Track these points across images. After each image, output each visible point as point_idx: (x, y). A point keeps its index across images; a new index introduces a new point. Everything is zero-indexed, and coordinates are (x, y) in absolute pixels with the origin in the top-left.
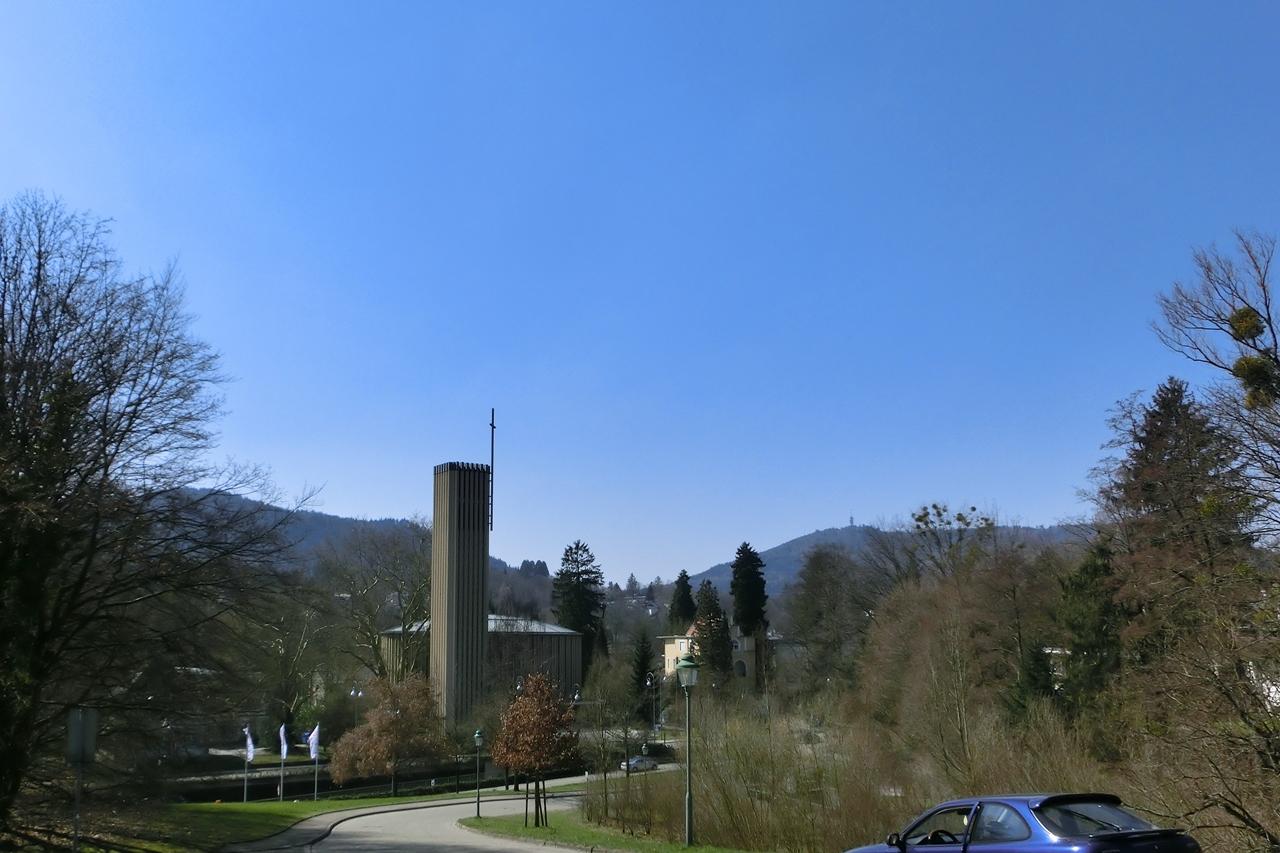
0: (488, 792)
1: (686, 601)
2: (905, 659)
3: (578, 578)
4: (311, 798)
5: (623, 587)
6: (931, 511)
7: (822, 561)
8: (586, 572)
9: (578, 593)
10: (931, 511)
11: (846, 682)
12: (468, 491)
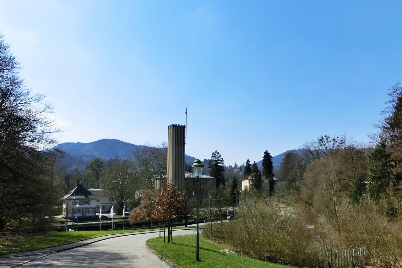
0: (183, 227)
1: (249, 169)
2: (315, 184)
3: (216, 162)
4: (122, 229)
5: (233, 167)
6: (324, 138)
7: (289, 156)
8: (219, 160)
9: (215, 167)
10: (324, 138)
11: (296, 192)
12: (178, 134)
